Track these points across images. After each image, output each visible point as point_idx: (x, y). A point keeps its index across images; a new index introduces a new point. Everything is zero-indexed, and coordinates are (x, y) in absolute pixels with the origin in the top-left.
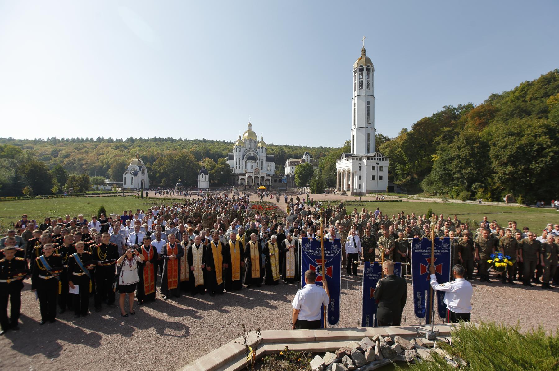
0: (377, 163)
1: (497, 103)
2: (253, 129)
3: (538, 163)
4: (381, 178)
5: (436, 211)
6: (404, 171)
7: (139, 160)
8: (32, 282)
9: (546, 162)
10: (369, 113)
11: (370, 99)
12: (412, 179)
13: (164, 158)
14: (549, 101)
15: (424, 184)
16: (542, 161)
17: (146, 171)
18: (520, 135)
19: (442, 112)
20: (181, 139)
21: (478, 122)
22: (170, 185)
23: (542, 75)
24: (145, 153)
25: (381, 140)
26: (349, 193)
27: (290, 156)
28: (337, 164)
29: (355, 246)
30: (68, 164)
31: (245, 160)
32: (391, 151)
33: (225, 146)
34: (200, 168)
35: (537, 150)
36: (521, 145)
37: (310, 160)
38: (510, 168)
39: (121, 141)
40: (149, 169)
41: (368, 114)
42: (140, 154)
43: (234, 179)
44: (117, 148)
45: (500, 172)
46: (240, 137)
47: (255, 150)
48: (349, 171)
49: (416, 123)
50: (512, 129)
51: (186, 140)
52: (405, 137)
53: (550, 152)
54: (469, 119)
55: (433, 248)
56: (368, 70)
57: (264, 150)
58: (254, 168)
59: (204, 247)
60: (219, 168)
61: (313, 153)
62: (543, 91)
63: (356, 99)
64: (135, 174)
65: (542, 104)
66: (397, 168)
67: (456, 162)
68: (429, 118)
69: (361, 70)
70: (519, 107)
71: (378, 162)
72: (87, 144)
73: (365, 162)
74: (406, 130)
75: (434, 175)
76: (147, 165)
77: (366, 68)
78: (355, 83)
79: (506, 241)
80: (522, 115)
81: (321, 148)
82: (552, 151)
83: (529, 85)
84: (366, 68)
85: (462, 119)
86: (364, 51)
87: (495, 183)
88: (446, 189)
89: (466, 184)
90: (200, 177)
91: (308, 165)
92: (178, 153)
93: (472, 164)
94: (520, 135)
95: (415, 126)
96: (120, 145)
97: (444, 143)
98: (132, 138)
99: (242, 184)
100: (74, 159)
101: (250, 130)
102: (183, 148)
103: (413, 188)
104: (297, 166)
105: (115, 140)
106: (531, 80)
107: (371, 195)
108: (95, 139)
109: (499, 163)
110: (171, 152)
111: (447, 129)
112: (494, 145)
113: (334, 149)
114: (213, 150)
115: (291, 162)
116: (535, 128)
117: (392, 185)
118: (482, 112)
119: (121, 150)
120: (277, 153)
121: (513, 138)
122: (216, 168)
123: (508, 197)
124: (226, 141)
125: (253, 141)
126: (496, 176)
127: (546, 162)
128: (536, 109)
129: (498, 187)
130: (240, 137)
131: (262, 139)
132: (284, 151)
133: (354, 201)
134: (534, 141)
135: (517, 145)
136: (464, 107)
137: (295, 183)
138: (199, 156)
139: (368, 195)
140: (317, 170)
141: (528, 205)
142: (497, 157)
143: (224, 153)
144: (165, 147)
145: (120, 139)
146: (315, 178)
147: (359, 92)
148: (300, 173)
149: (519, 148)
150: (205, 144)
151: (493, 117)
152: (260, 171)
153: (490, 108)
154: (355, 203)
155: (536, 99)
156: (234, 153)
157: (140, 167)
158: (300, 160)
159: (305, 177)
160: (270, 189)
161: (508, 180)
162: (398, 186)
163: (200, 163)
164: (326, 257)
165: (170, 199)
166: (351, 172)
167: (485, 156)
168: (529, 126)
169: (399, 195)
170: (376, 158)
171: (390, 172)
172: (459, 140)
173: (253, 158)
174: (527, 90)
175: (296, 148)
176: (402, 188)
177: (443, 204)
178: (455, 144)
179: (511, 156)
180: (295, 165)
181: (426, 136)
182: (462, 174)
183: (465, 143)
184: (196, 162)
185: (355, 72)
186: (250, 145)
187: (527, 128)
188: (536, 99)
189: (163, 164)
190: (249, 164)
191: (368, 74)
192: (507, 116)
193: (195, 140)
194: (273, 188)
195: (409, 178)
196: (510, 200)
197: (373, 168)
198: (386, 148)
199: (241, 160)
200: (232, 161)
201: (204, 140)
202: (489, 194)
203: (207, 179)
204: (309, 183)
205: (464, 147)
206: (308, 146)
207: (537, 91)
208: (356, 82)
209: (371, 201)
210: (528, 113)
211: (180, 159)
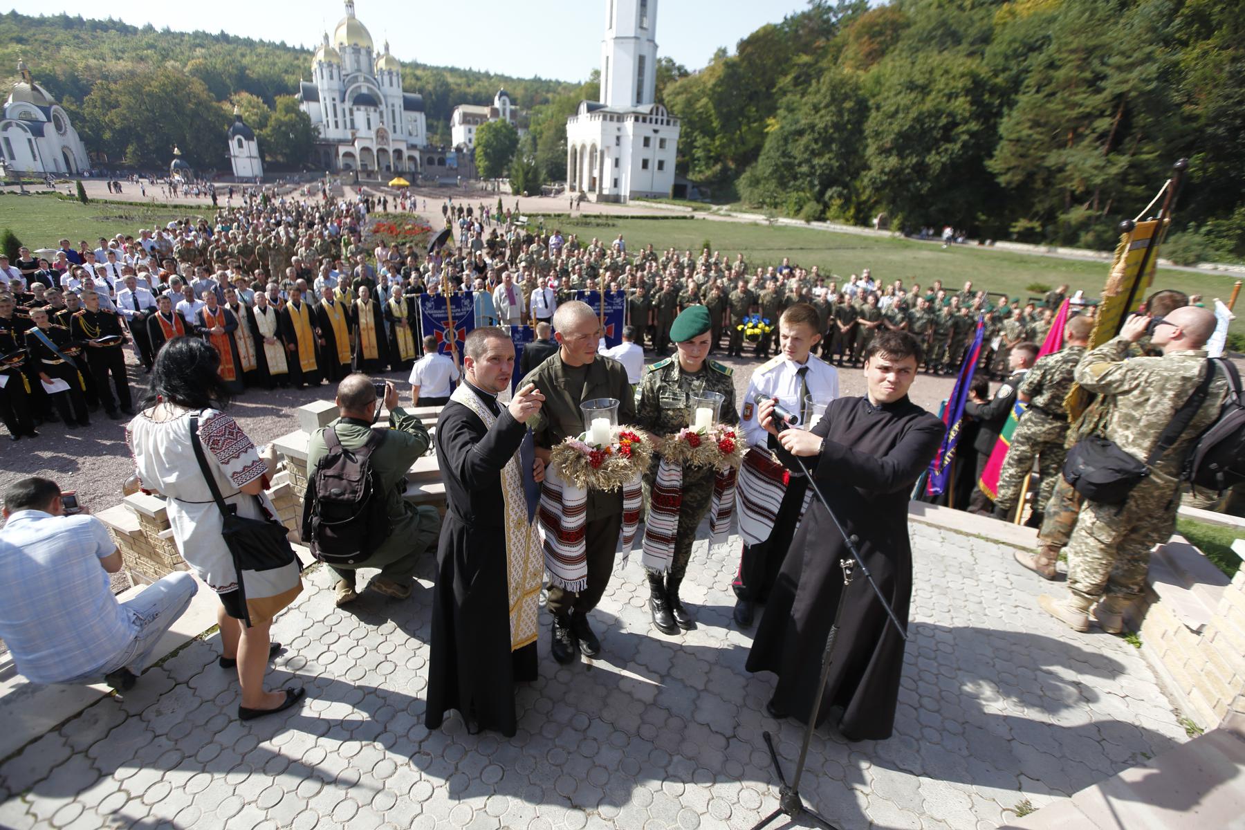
0: (656, 131)
2: (361, 17)
4: (661, 165)
5: (756, 237)
6: (710, 151)
7: (34, 88)
12: (725, 169)
13: (112, 86)
15: (742, 184)
16: (946, 150)
17: (68, 122)
18: (924, 90)
19: (803, 14)
20: (150, 29)
21: (866, 49)
22: (154, 168)
25: (668, 73)
26: (592, 197)
27: (464, 100)
29: (546, 306)
31: (348, 105)
32: (689, 103)
33: (287, 58)
34: (230, 120)
36: (921, 114)
38: (893, 161)
40: (75, 117)
42: (30, 66)
43: (327, 154)
46: (326, 37)
47: (371, 77)
48: (594, 147)
49: (745, 37)
51: (167, 32)
52: (720, 71)
55: (449, 306)
57: (395, 79)
58: (374, 128)
59: (276, 312)
60: (280, 124)
61: (519, 92)
66: (697, 144)
67: (804, 140)
68: (775, 26)
71: (657, 127)
73: (629, 124)
75: (763, 166)
76: (65, 104)
79: (768, 298)
80: (944, 43)
81: (537, 80)
85: (841, 33)
88: (782, 196)
89: (817, 188)
90: (233, 144)
91: (505, 126)
94: (924, 90)
95: (743, 45)
97: (794, 93)
99: (348, 167)
101: (352, 17)
102: (165, 57)
103: (720, 191)
104: (480, 127)
107: (637, 202)
110: (130, 65)
111: (805, 58)
113: (568, 87)
114: (257, 70)
117: (683, 182)
118: (877, 24)
121: (912, 96)
122: (272, 122)
123: (881, 219)
124: (289, 45)
125: (363, 52)
128: (973, 32)
130: (326, 37)
131: (387, 48)
132: (446, 84)
133: (595, 217)
135: (913, 113)
137: (477, 168)
139: (632, 203)
140: (523, 136)
141: (908, 235)
142: (877, 134)
143: (290, 79)
144: (105, 49)
146: (519, 159)
148: (487, 145)
149: (919, 120)
150: (228, 47)
151: (896, 40)
152: (391, 136)
153: (896, 16)
154: (600, 221)
157: (46, 111)
158: (486, 110)
159: (499, 154)
160: (419, 182)
161: (885, 184)
162: (696, 185)
163: (226, 106)
164: (454, 318)
165: (165, 206)
166: (599, 148)
167: (858, 131)
169: (694, 204)
170: (654, 117)
171: (680, 152)
172: (818, 91)
173: (368, 101)
176: (703, 189)
177: (768, 227)
178: (810, 99)
179: (900, 134)
180: (476, 123)
181: (763, 66)
182: (813, 167)
183: (828, 99)
184: (215, 104)
186: (358, 62)
189: (116, 105)
190: (360, 116)
192: (920, 41)
193: (196, 35)
194: (425, 178)
195: (718, 167)
196: (884, 225)
197: (647, 141)
198: (678, 94)
199: (338, 102)
200: (313, 105)
201: (224, 37)
202: (852, 211)
203: (255, 152)
204: (509, 170)
205: (827, 106)
206: (507, 74)
209: (633, 217)
210: (956, 39)
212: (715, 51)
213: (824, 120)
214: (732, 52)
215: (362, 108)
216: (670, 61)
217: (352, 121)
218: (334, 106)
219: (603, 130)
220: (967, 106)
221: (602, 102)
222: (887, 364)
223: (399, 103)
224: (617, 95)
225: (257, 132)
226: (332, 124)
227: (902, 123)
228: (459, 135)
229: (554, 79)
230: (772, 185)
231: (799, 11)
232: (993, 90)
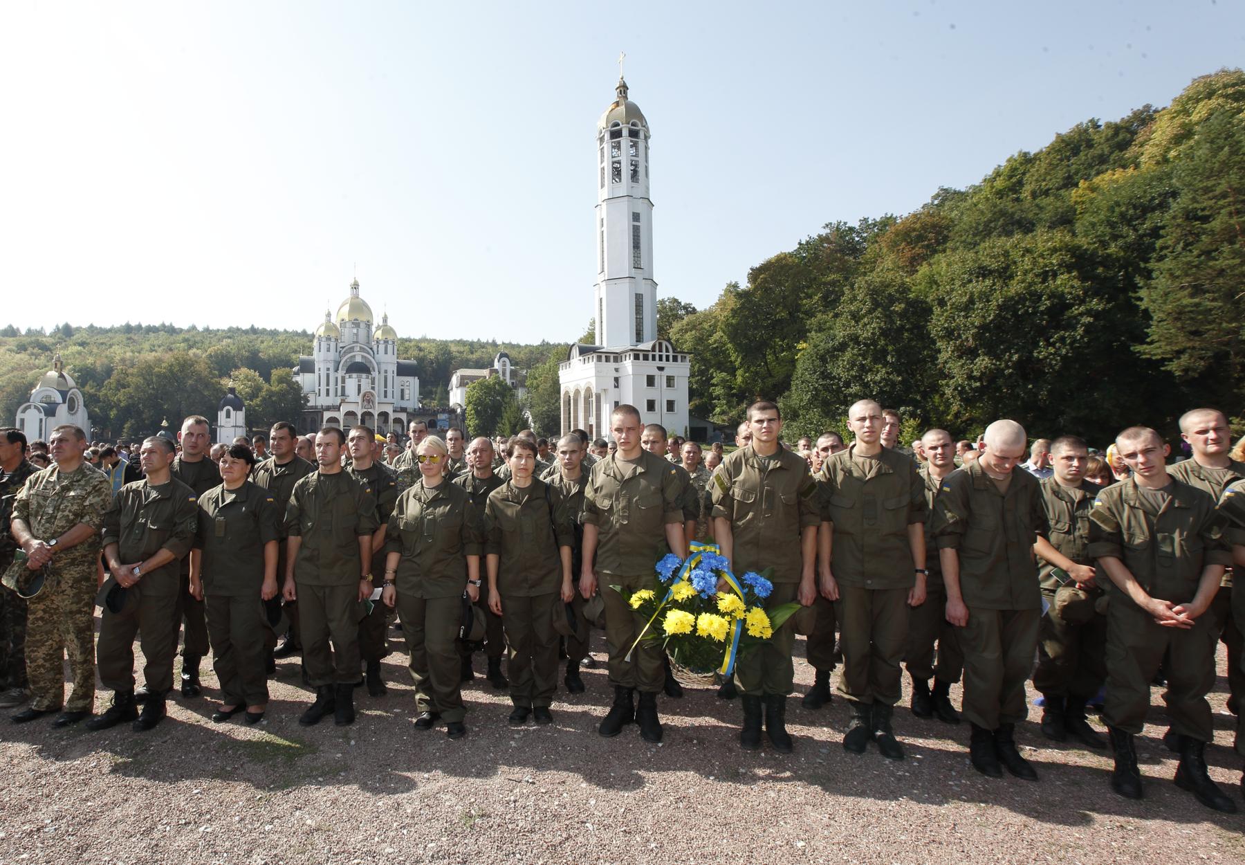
0: (661, 369)
1: (951, 210)
2: (363, 295)
3: (1053, 345)
4: (671, 405)
6: (731, 388)
7: (61, 376)
8: (164, 706)
9: (1074, 341)
11: (640, 207)
14: (1074, 194)
16: (1062, 340)
18: (1005, 274)
23: (1059, 135)
24: (90, 360)
25: (672, 312)
27: (466, 364)
28: (561, 373)
31: (341, 373)
32: (700, 340)
33: (301, 341)
36: (1008, 299)
37: (512, 371)
38: (983, 362)
39: (40, 333)
40: (90, 401)
41: (636, 245)
44: (22, 348)
45: (957, 372)
46: (329, 315)
48: (588, 390)
50: (987, 262)
51: (207, 330)
52: (732, 303)
53: (1081, 314)
54: (885, 250)
56: (634, 134)
61: (513, 354)
62: (1061, 174)
63: (604, 205)
64: (50, 411)
65: (1059, 204)
67: (848, 354)
69: (616, 134)
70: (1003, 213)
71: (663, 363)
73: (628, 364)
74: (736, 286)
76: (87, 388)
77: (629, 128)
78: (603, 169)
82: (1088, 313)
83: (1027, 160)
84: (629, 128)
86: (623, 89)
87: (948, 405)
90: (222, 415)
94: (1005, 274)
95: (755, 274)
96: (35, 344)
102: (190, 347)
105: (23, 332)
106: (1033, 150)
109: (957, 349)
112: (942, 303)
115: (463, 378)
116: (1042, 256)
117: (702, 424)
118: (914, 230)
119: (32, 354)
120: (432, 356)
121: (988, 282)
125: (362, 325)
126: (947, 385)
127: (1074, 341)
129: (957, 415)
130: (329, 315)
131: (385, 319)
132: (450, 353)
134: (1039, 288)
135: (997, 299)
136: (875, 225)
138: (224, 364)
142: (949, 334)
145: (38, 328)
155: (1046, 193)
156: (316, 356)
157: (64, 394)
166: (594, 391)
168: (1028, 251)
170: (657, 353)
171: (692, 393)
173: (360, 368)
174: (1024, 174)
179: (984, 327)
181: (781, 300)
183: (869, 304)
185: (602, 139)
187: (1023, 256)
188: (1046, 193)
190: (352, 383)
191: (635, 145)
192: (975, 235)
193: (230, 330)
197: (651, 381)
205: (870, 312)
206: (514, 342)
207: (1047, 174)
208: (605, 164)
210: (1027, 227)
211: (171, 371)
213: (869, 329)
214: (744, 285)
215: (354, 375)
216: (676, 301)
217: (343, 388)
218: (328, 376)
219: (598, 372)
220: (1076, 283)
221: (597, 344)
222: (1071, 453)
223: (393, 368)
224: (616, 337)
225: (246, 403)
226: (323, 392)
228: (457, 397)
229: (562, 343)
230: (815, 414)
232: (1107, 261)
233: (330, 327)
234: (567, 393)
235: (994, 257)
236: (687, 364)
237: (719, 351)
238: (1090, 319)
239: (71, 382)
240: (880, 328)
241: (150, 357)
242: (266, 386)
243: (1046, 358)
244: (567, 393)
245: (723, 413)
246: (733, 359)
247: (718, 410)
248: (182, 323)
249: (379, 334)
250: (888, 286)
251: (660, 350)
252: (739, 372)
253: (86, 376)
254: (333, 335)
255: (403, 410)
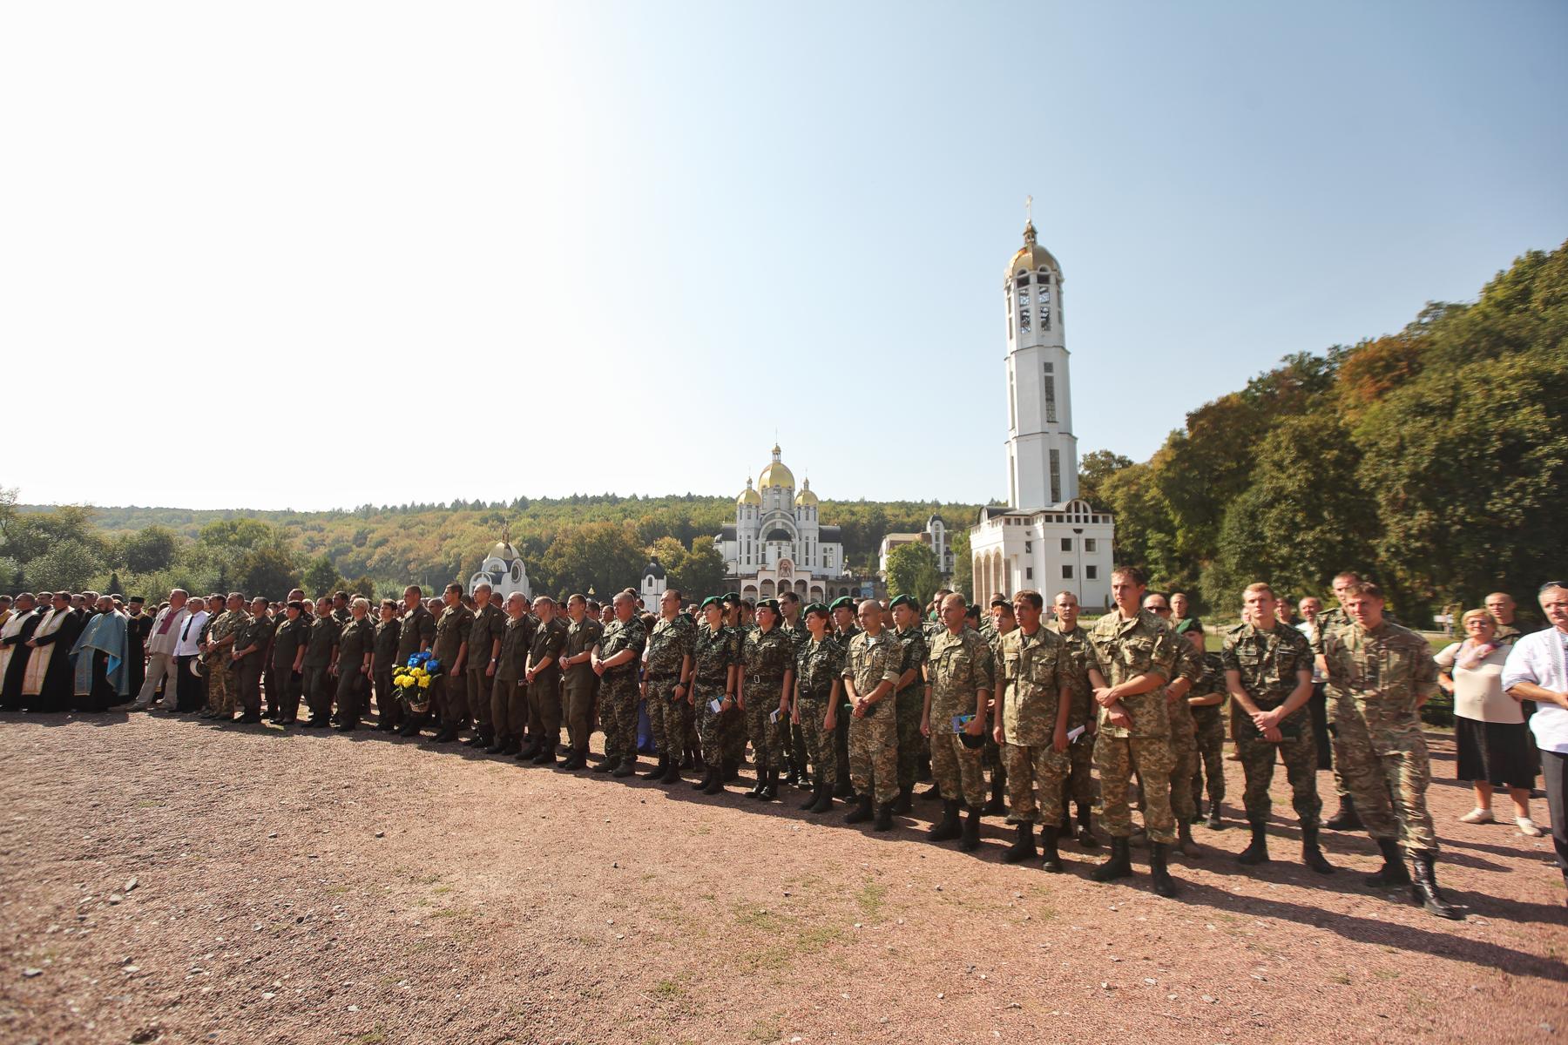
0: (1078, 531)
3: (1510, 494)
4: (1091, 572)
6: (1171, 551)
7: (508, 547)
9: (1539, 489)
10: (1052, 391)
11: (1053, 356)
18: (1448, 411)
24: (537, 532)
25: (1105, 464)
27: (900, 529)
28: (972, 537)
30: (382, 560)
31: (762, 540)
35: (1499, 454)
38: (1422, 517)
39: (502, 506)
40: (532, 570)
44: (485, 521)
46: (750, 482)
48: (998, 555)
51: (646, 499)
53: (1548, 456)
56: (1043, 280)
60: (692, 562)
61: (945, 514)
69: (1023, 282)
72: (428, 517)
73: (1039, 526)
77: (1039, 273)
83: (1538, 260)
84: (1039, 273)
86: (1031, 233)
90: (644, 583)
92: (592, 526)
93: (1326, 514)
95: (1193, 419)
96: (494, 516)
98: (524, 499)
100: (394, 550)
101: (777, 463)
108: (448, 506)
116: (1502, 386)
118: (1381, 359)
120: (864, 521)
121: (1426, 422)
130: (750, 482)
131: (807, 483)
132: (883, 517)
135: (1432, 444)
138: (653, 533)
147: (1020, 340)
149: (1439, 450)
157: (509, 563)
158: (918, 537)
168: (1486, 381)
170: (1073, 514)
173: (780, 535)
175: (922, 507)
179: (1415, 476)
181: (1218, 445)
183: (1294, 453)
185: (1008, 289)
190: (771, 551)
193: (668, 498)
197: (1066, 545)
199: (752, 539)
200: (730, 544)
205: (1293, 462)
208: (1013, 314)
212: (1168, 435)
216: (1108, 454)
220: (1540, 418)
223: (814, 535)
226: (744, 560)
227: (1421, 458)
231: (1267, 371)
233: (750, 493)
234: (978, 559)
235: (1438, 391)
236: (1111, 525)
237: (1158, 509)
238: (1559, 462)
239: (515, 553)
240: (1307, 480)
241: (583, 528)
242: (687, 555)
243: (1501, 511)
244: (978, 559)
245: (1162, 580)
246: (1171, 517)
247: (1156, 576)
248: (624, 493)
249: (800, 500)
250: (1321, 429)
251: (1077, 511)
252: (1179, 533)
253: (534, 546)
254: (754, 502)
255: (824, 578)
